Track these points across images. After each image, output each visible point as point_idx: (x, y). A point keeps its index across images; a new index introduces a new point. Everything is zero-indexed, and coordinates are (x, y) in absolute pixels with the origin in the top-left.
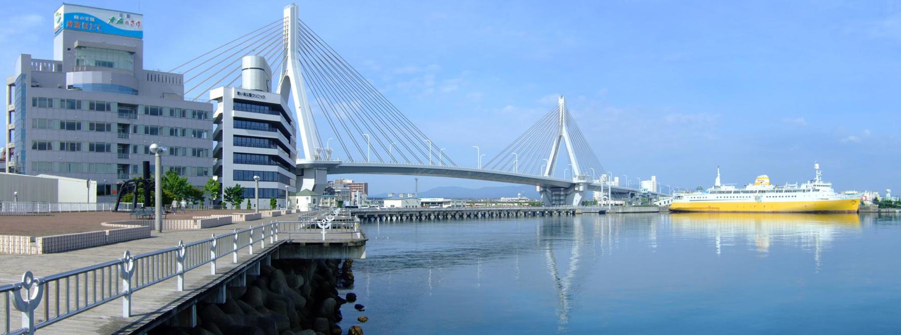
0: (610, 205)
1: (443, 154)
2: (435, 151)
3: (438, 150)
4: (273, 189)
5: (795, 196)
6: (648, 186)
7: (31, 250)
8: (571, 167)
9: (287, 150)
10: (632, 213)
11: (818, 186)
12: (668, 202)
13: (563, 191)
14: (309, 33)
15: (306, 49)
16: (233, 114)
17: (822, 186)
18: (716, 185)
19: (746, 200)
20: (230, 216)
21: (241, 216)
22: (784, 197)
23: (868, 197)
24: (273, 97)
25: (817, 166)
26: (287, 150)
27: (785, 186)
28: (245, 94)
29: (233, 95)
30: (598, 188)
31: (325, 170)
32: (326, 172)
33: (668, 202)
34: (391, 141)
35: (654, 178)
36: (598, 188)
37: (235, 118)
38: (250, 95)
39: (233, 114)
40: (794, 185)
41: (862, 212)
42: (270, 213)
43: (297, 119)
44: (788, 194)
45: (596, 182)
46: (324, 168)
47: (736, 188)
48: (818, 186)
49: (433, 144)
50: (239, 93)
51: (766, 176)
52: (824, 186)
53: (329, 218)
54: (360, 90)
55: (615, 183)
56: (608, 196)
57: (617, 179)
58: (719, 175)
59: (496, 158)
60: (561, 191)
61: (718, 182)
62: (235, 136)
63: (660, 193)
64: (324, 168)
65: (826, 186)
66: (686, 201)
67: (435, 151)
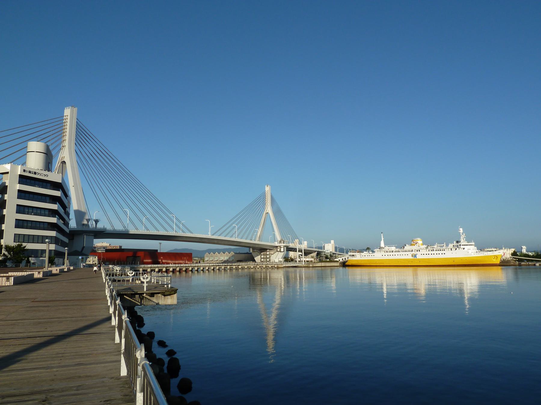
0: (303, 261)
1: (183, 225)
2: (178, 223)
3: (180, 222)
4: (24, 235)
5: (445, 254)
6: (329, 248)
7: (5, 283)
8: (274, 235)
9: (63, 219)
10: (320, 267)
11: (463, 245)
12: (345, 259)
13: (269, 251)
14: (85, 131)
15: (84, 137)
16: (18, 187)
17: (466, 245)
18: (381, 246)
19: (405, 256)
20: (32, 273)
21: (39, 273)
22: (425, 254)
23: (507, 253)
24: (54, 177)
25: (461, 230)
26: (63, 219)
27: (435, 246)
28: (30, 172)
29: (19, 171)
30: (294, 250)
31: (92, 235)
32: (93, 237)
33: (345, 259)
34: (144, 215)
35: (332, 242)
36: (294, 250)
37: (19, 191)
38: (35, 173)
39: (18, 187)
40: (443, 245)
41: (504, 264)
42: (57, 270)
43: (70, 189)
44: (438, 252)
45: (291, 245)
46: (92, 234)
47: (396, 248)
48: (463, 245)
49: (177, 219)
50: (24, 171)
51: (419, 239)
52: (468, 245)
53: (144, 278)
54: (122, 176)
55: (304, 246)
56: (302, 255)
57: (306, 243)
58: (383, 239)
59: (219, 230)
60: (267, 252)
61: (382, 245)
62: (17, 205)
63: (338, 253)
64: (92, 234)
65: (470, 245)
66: (359, 257)
67: (178, 223)
